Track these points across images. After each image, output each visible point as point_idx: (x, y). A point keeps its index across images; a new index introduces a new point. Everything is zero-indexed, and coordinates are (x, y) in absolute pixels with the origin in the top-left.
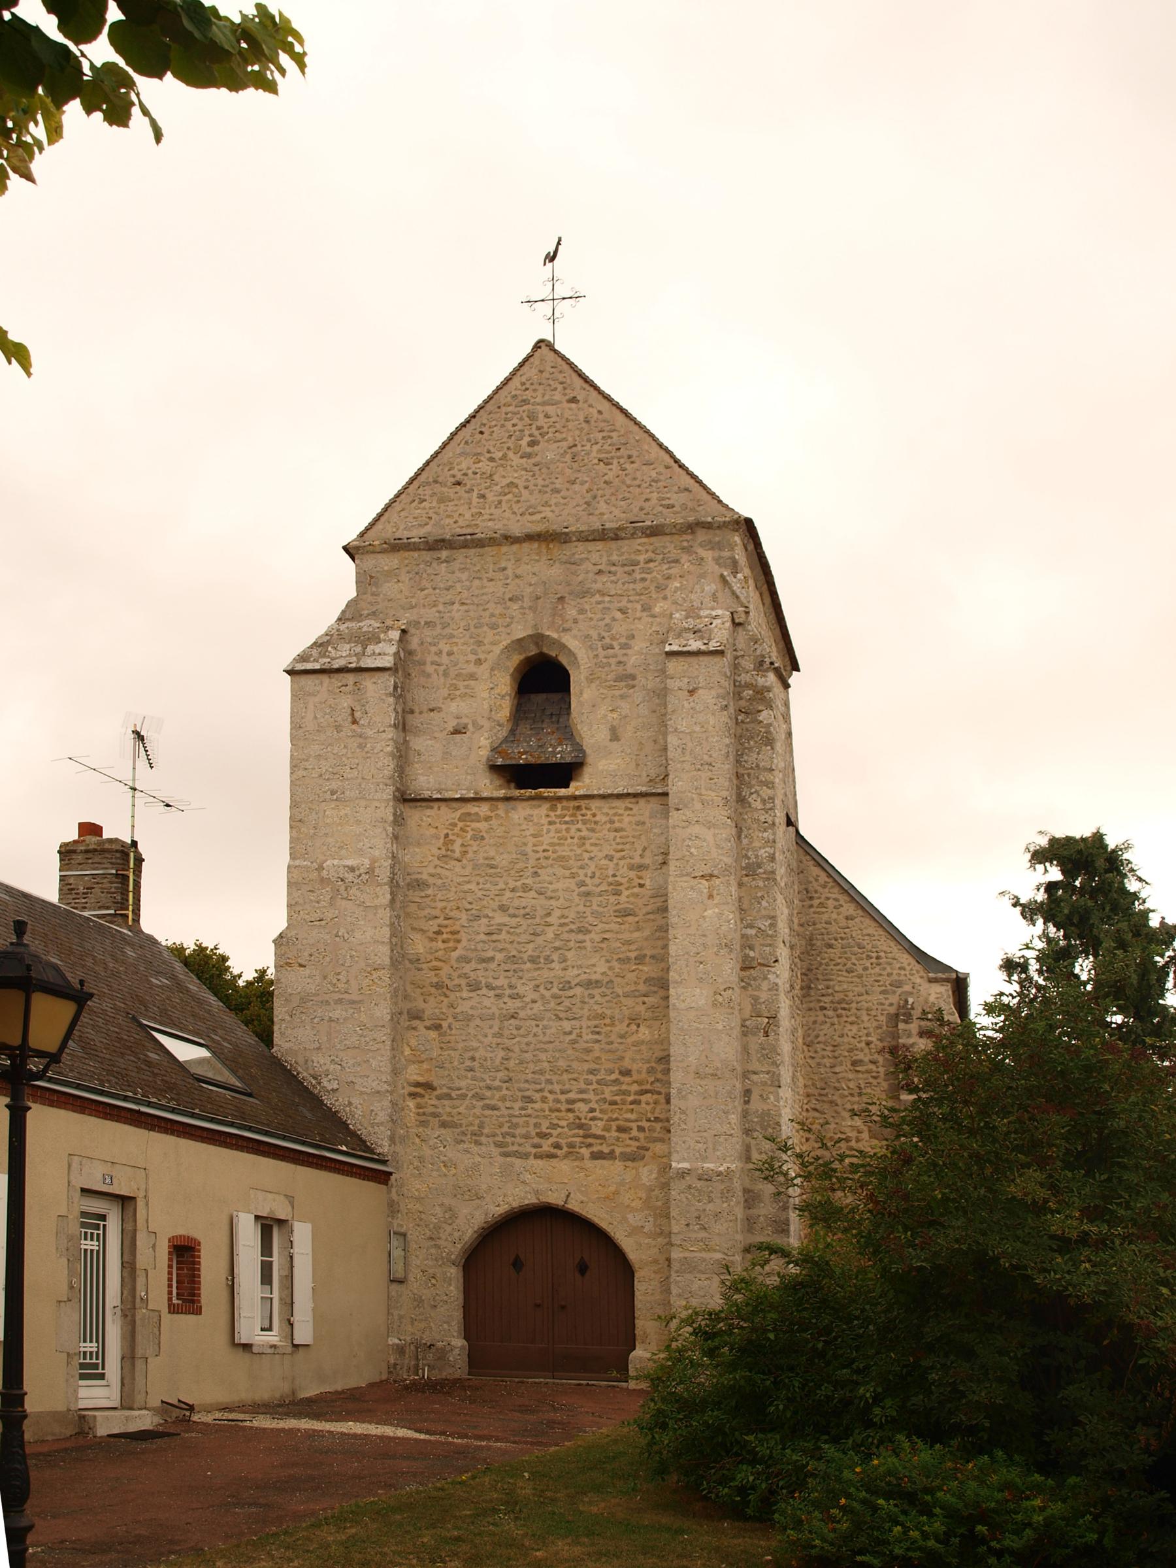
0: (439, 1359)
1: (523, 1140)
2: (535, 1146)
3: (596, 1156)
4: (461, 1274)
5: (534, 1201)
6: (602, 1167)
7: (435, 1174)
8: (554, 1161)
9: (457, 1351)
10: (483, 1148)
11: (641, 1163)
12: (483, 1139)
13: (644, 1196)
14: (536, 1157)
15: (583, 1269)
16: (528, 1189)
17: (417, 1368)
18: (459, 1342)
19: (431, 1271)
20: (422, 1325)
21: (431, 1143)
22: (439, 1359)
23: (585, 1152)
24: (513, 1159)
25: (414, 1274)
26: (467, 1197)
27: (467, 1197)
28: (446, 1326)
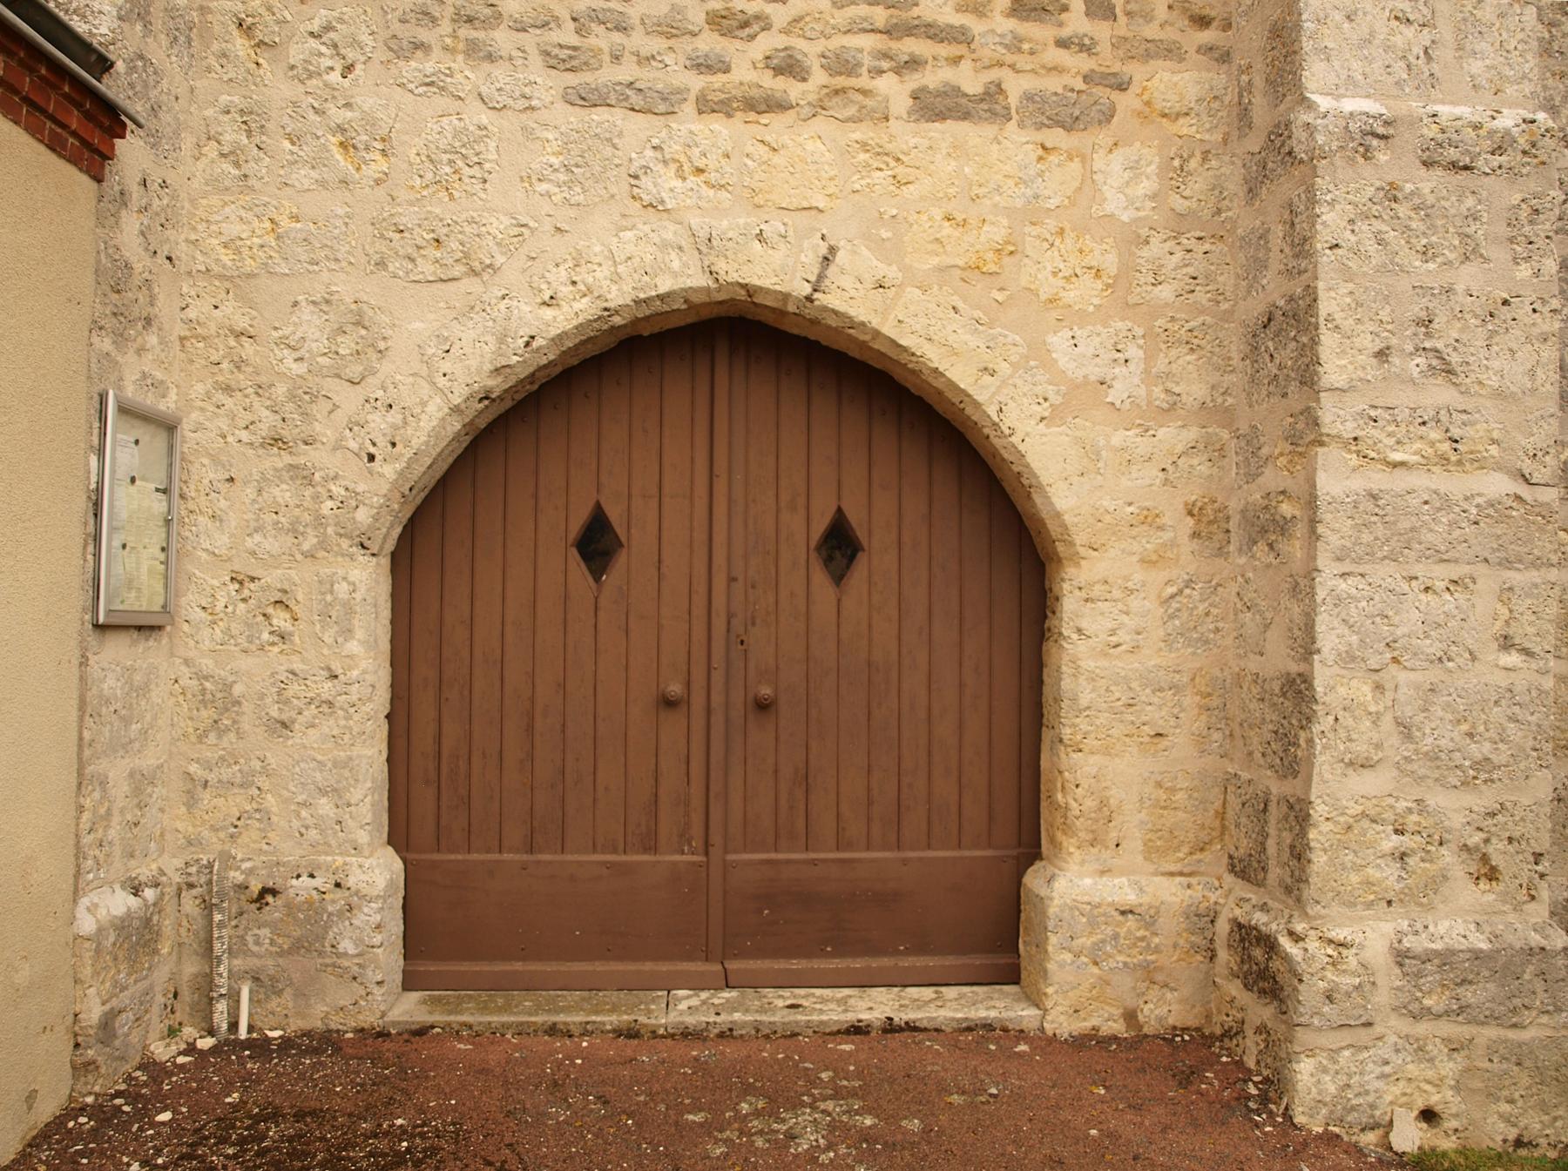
0: (297, 947)
1: (656, 44)
2: (703, 66)
3: (936, 107)
4: (385, 587)
5: (696, 279)
6: (958, 150)
7: (303, 176)
8: (777, 121)
9: (369, 914)
10: (500, 72)
11: (1103, 137)
12: (502, 39)
13: (1111, 263)
14: (706, 106)
15: (839, 545)
16: (670, 232)
17: (206, 989)
18: (378, 872)
19: (273, 577)
20: (235, 803)
21: (296, 54)
22: (297, 947)
23: (894, 90)
24: (617, 116)
25: (206, 587)
26: (426, 269)
27: (426, 269)
28: (325, 806)
